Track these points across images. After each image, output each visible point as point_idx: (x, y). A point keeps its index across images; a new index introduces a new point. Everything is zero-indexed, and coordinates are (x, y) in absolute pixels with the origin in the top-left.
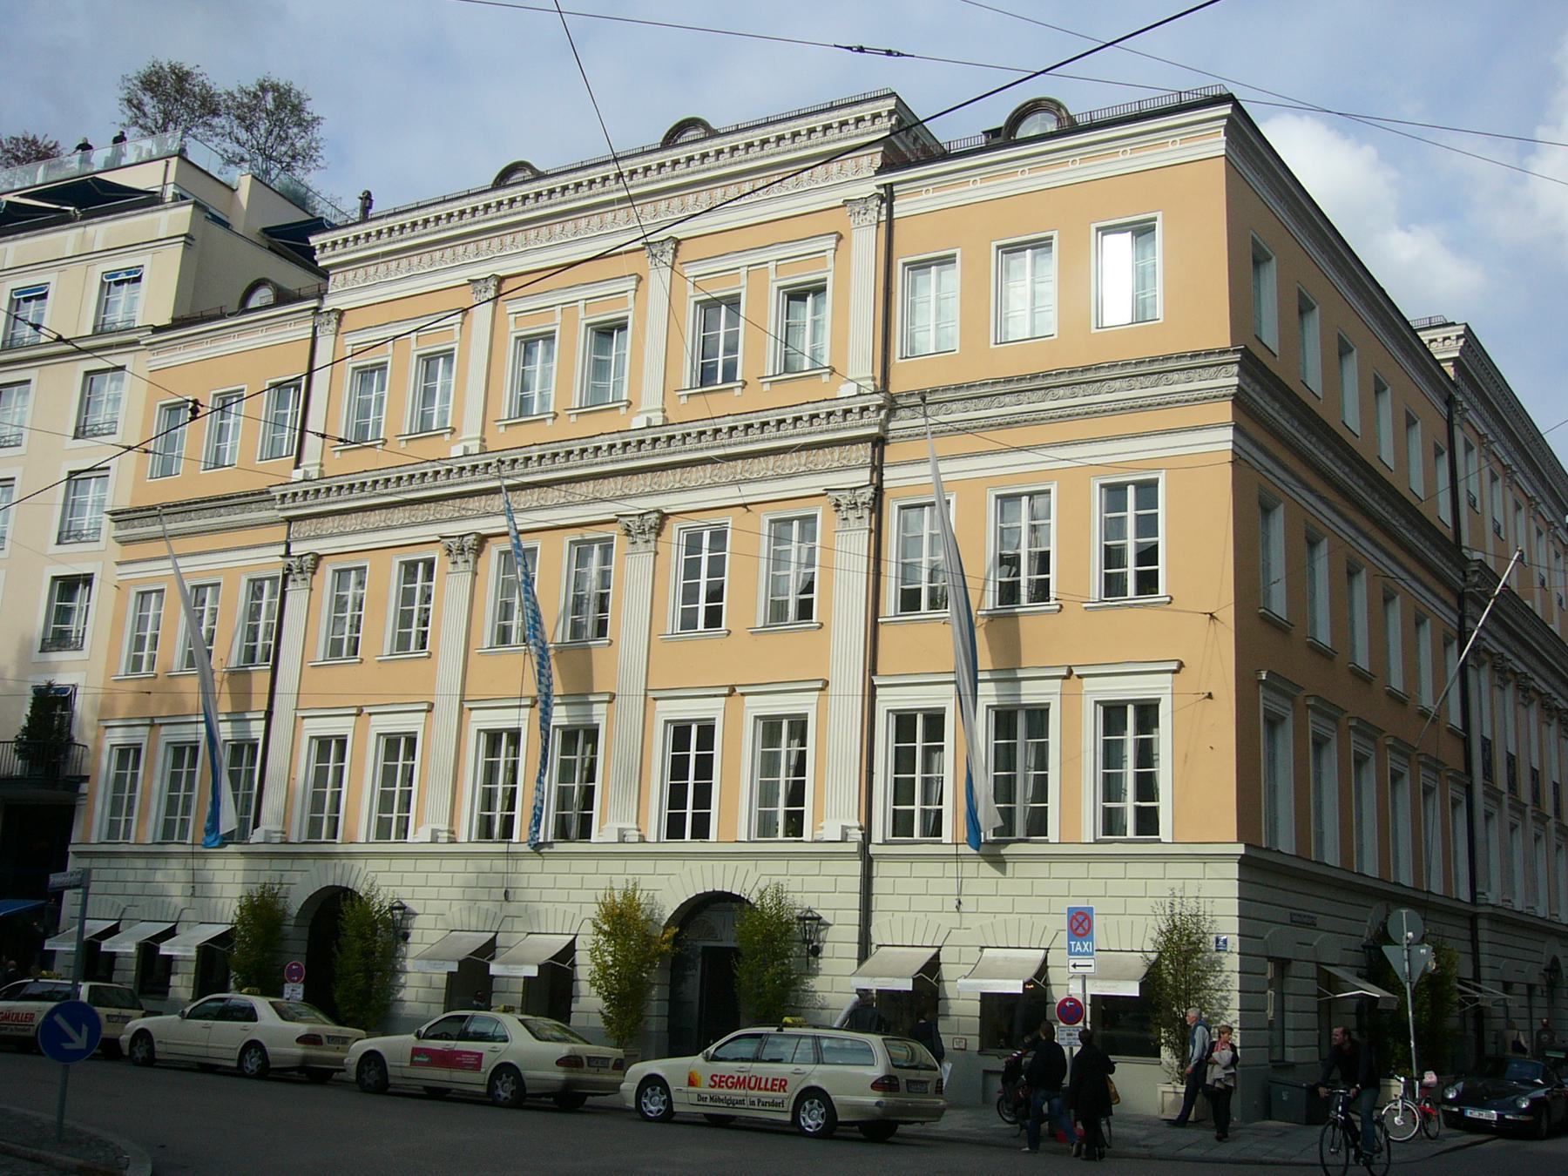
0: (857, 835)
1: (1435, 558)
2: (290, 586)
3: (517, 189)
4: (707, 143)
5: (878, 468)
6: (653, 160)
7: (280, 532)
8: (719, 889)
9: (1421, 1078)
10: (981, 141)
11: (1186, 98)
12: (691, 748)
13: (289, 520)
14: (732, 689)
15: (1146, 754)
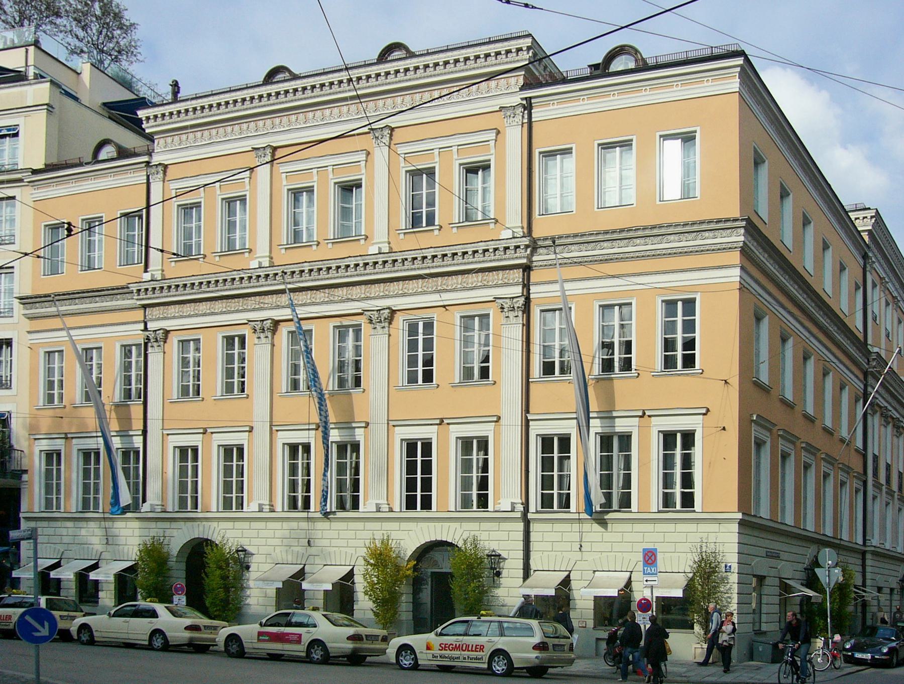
0: (520, 508)
1: (852, 350)
2: (150, 350)
3: (281, 85)
4: (408, 61)
5: (526, 285)
6: (256, 92)
7: (139, 315)
11: (716, 52)
12: (418, 456)
13: (145, 307)
14: (442, 420)
15: (687, 462)
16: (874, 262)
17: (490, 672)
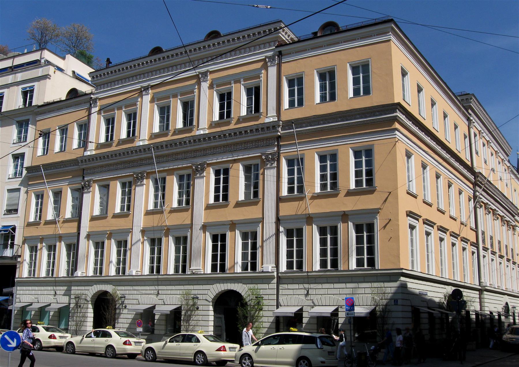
1: (465, 171)
6: (201, 45)
8: (238, 291)
9: (354, 334)
10: (311, 36)
11: (377, 21)
16: (474, 122)
17: (194, 363)
